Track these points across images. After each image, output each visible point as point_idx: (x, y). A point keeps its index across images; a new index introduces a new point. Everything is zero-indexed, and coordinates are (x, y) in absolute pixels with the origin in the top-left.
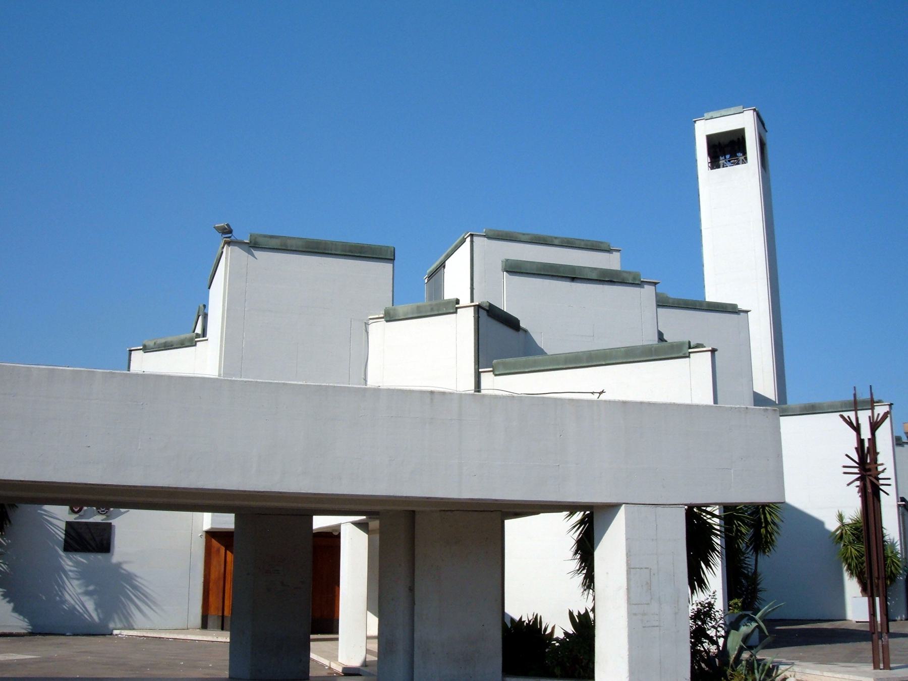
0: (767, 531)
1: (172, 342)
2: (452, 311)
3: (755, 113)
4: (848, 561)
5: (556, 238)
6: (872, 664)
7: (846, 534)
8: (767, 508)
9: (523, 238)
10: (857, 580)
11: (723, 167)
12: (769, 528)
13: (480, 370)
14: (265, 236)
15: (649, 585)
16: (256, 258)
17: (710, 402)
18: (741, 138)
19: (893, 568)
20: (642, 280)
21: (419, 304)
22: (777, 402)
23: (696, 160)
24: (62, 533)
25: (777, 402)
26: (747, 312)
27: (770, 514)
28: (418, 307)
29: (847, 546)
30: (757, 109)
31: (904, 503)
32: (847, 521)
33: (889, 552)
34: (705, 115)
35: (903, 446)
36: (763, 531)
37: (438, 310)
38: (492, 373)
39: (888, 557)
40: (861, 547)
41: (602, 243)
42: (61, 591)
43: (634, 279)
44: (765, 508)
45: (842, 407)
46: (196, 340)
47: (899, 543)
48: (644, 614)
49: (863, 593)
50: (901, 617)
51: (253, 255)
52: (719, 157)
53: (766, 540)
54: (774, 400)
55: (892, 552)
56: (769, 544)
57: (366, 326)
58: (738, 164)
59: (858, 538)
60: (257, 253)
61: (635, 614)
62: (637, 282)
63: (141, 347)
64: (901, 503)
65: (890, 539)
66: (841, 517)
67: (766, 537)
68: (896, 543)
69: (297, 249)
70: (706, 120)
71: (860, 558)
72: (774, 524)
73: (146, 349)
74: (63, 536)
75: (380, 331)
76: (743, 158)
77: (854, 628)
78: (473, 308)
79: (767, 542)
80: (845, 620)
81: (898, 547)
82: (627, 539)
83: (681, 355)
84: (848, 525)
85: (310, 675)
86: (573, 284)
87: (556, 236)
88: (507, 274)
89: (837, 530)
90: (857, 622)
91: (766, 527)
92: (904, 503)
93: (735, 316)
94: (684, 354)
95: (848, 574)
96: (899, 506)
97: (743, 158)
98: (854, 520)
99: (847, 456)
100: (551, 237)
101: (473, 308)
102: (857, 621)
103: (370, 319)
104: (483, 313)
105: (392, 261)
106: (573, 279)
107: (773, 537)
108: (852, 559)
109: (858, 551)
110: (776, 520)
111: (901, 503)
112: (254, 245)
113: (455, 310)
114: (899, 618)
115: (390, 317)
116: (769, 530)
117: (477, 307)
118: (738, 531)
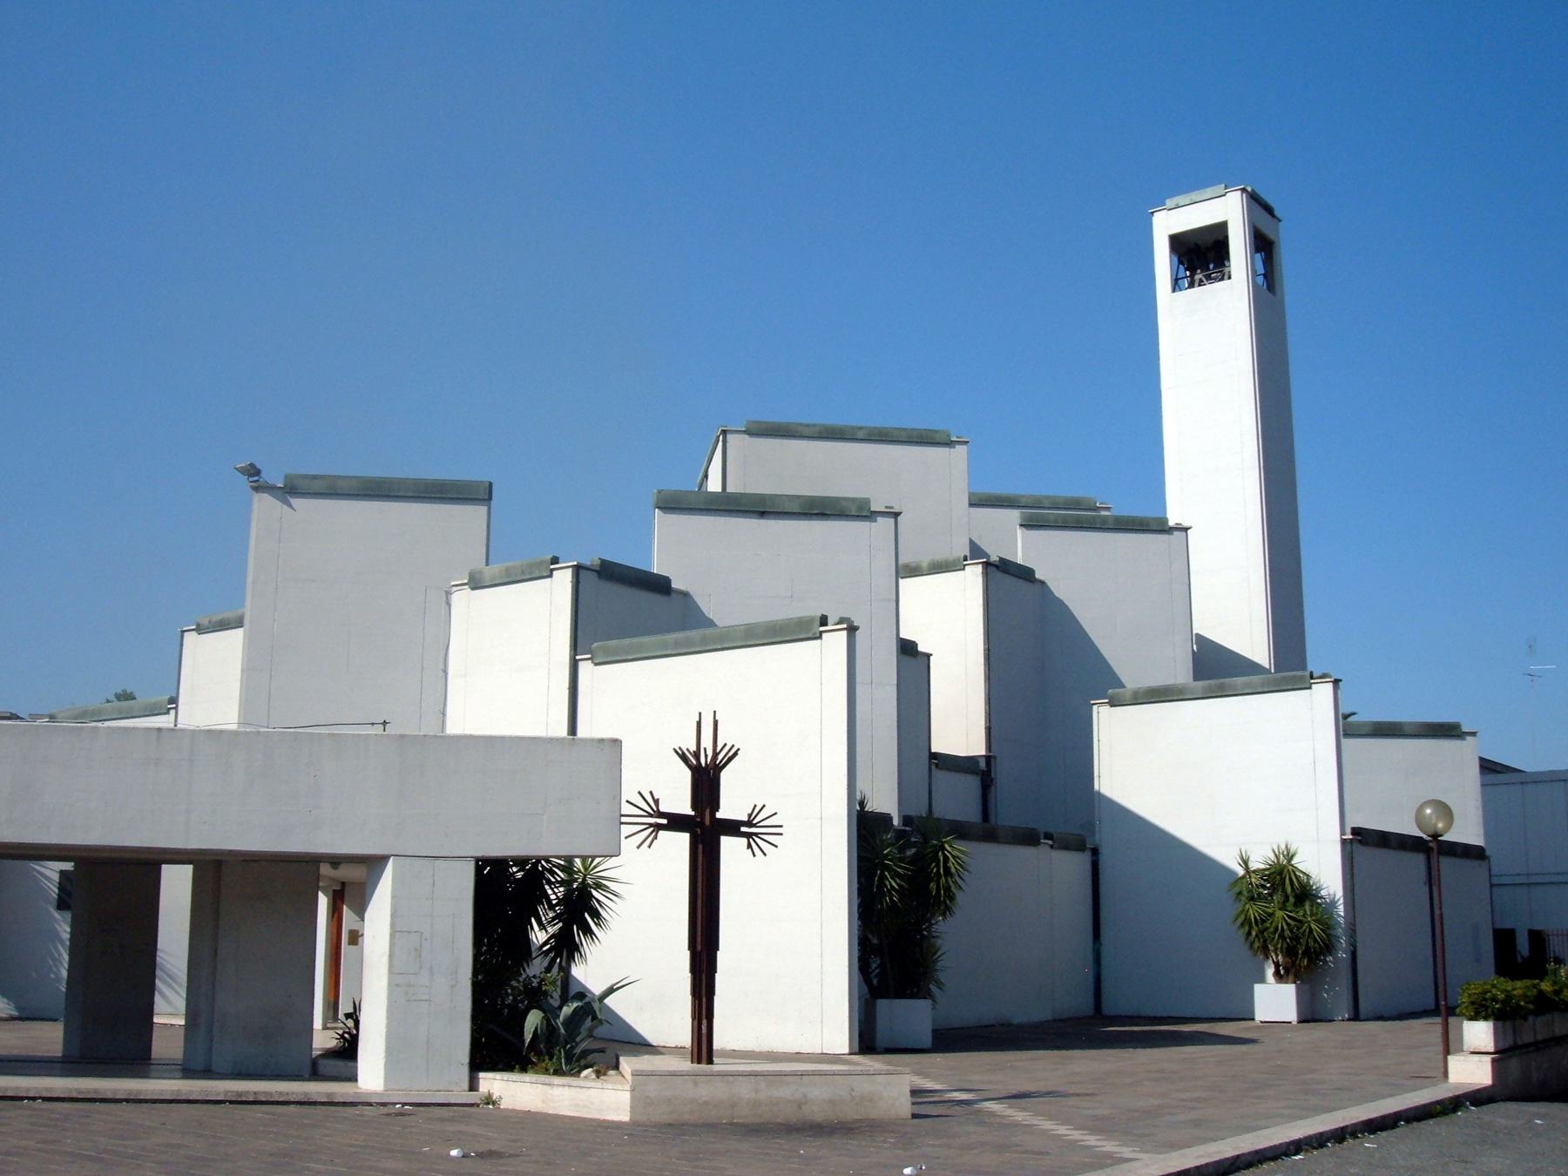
1: (228, 619)
2: (545, 574)
3: (1244, 195)
5: (861, 428)
6: (715, 1047)
9: (806, 432)
11: (1200, 285)
13: (578, 657)
14: (306, 477)
15: (418, 952)
16: (293, 509)
17: (562, 731)
21: (509, 564)
22: (1273, 671)
24: (54, 892)
25: (1273, 671)
26: (1186, 529)
28: (507, 569)
30: (1249, 189)
32: (1254, 866)
34: (1168, 201)
35: (1463, 739)
37: (530, 573)
38: (590, 661)
41: (937, 431)
42: (56, 966)
43: (860, 508)
46: (552, 567)
47: (1341, 901)
48: (409, 985)
51: (290, 505)
54: (1268, 667)
57: (447, 596)
58: (1222, 279)
60: (295, 502)
61: (398, 985)
62: (864, 514)
63: (194, 627)
65: (1329, 895)
66: (1245, 862)
69: (351, 492)
73: (200, 630)
74: (57, 891)
75: (463, 600)
78: (571, 569)
82: (393, 898)
83: (810, 635)
85: (625, 1117)
86: (762, 522)
87: (860, 424)
88: (661, 513)
90: (1262, 1022)
93: (1165, 537)
99: (640, 793)
100: (853, 428)
101: (571, 569)
103: (454, 586)
104: (589, 579)
105: (487, 503)
106: (763, 514)
112: (291, 490)
113: (549, 573)
115: (476, 583)
117: (575, 568)
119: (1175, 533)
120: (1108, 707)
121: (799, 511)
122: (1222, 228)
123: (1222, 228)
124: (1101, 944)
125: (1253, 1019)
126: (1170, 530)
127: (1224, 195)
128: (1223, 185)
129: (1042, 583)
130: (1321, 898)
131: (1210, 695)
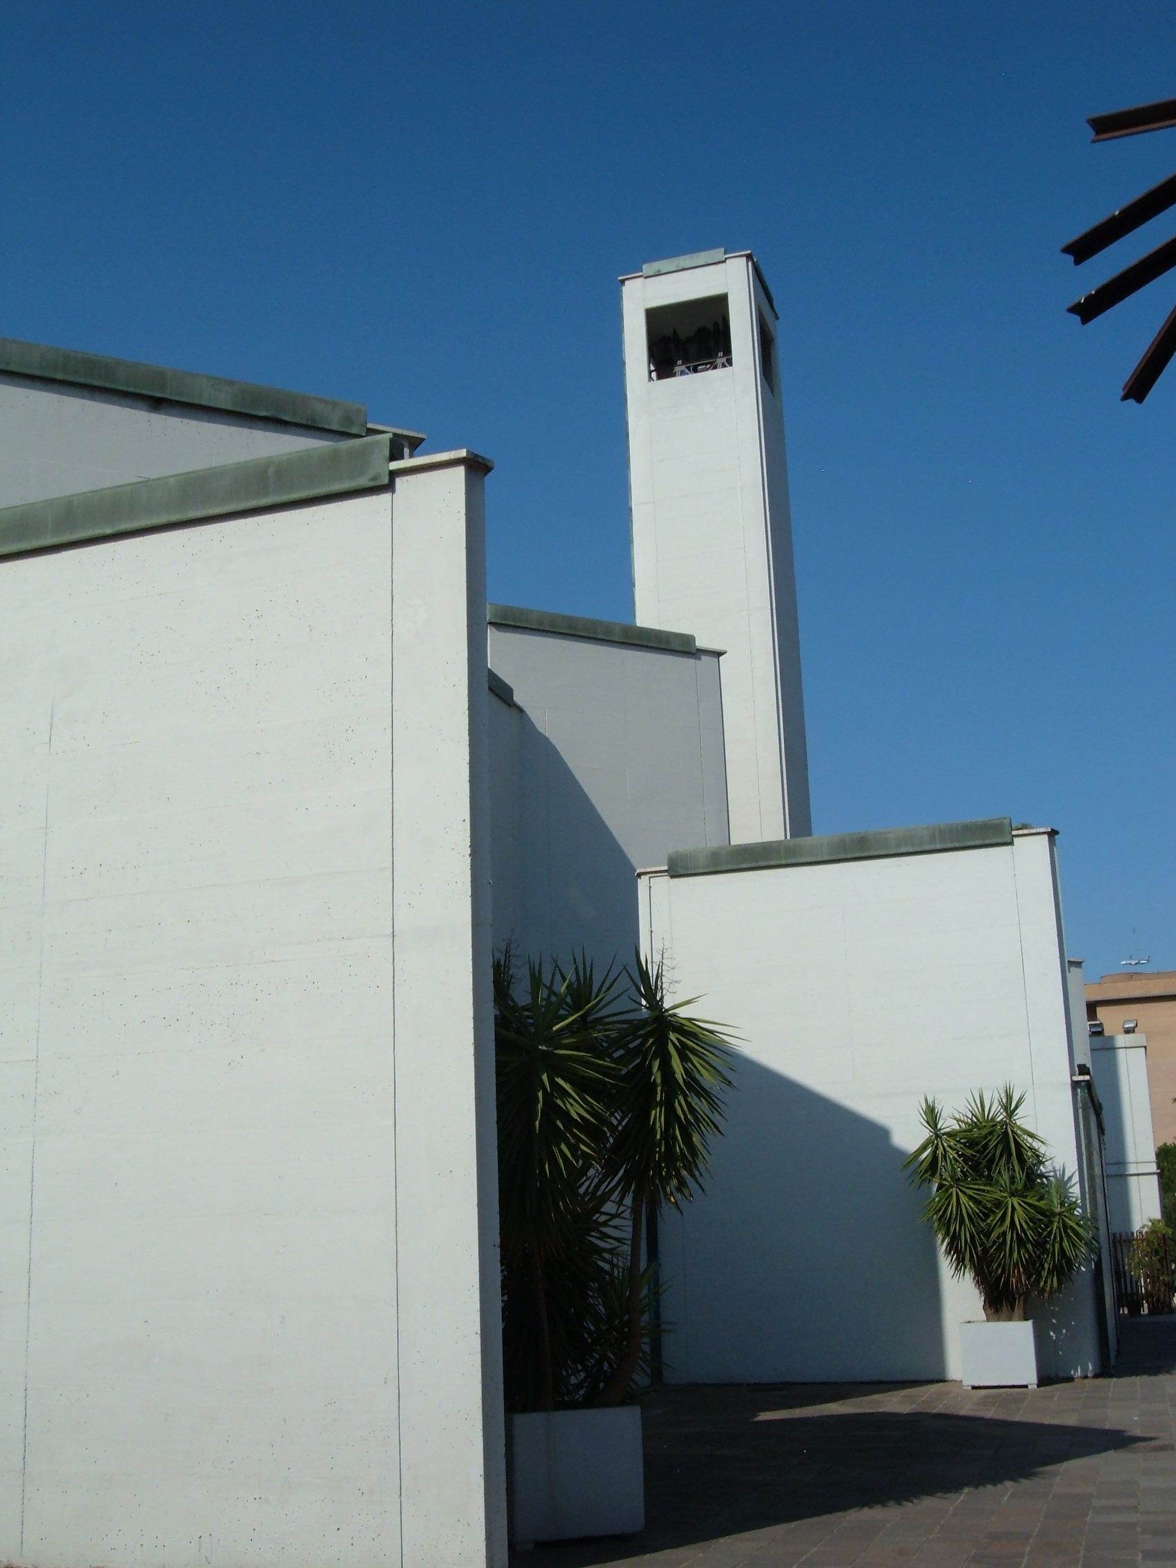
0: (671, 1116)
3: (750, 264)
4: (952, 1229)
7: (944, 1157)
8: (673, 1036)
10: (973, 1275)
12: (680, 1106)
18: (720, 322)
19: (1066, 1244)
20: (370, 426)
23: (624, 363)
26: (718, 654)
27: (684, 1058)
29: (947, 1191)
31: (1087, 1078)
32: (948, 1123)
33: (1056, 1201)
36: (657, 1116)
39: (1053, 1214)
40: (984, 1191)
43: (348, 420)
44: (667, 1038)
45: (933, 838)
47: (1076, 1178)
49: (990, 1312)
50: (1085, 1369)
52: (674, 364)
53: (670, 1148)
55: (1062, 1204)
56: (679, 1164)
59: (975, 1167)
64: (1081, 1078)
66: (931, 1115)
67: (668, 1135)
68: (1070, 1178)
70: (646, 277)
71: (983, 1221)
72: (702, 1092)
76: (724, 360)
77: (966, 1410)
79: (670, 1156)
80: (945, 1381)
81: (1075, 1191)
83: (363, 482)
84: (950, 1134)
89: (923, 1148)
90: (974, 1388)
91: (669, 1105)
92: (1087, 1078)
93: (690, 662)
94: (375, 479)
95: (1153, 1221)
96: (1075, 1085)
97: (724, 360)
98: (966, 1123)
102: (976, 1384)
106: (158, 404)
107: (696, 1139)
108: (962, 1222)
109: (977, 1202)
110: (707, 1079)
111: (1081, 1078)
114: (1079, 1373)
116: (680, 1112)
118: (553, 1111)
119: (703, 657)
120: (667, 878)
121: (229, 407)
122: (720, 302)
123: (720, 302)
124: (660, 1265)
125: (940, 1379)
126: (697, 653)
127: (723, 262)
128: (723, 249)
129: (521, 710)
130: (1042, 1176)
131: (843, 856)
